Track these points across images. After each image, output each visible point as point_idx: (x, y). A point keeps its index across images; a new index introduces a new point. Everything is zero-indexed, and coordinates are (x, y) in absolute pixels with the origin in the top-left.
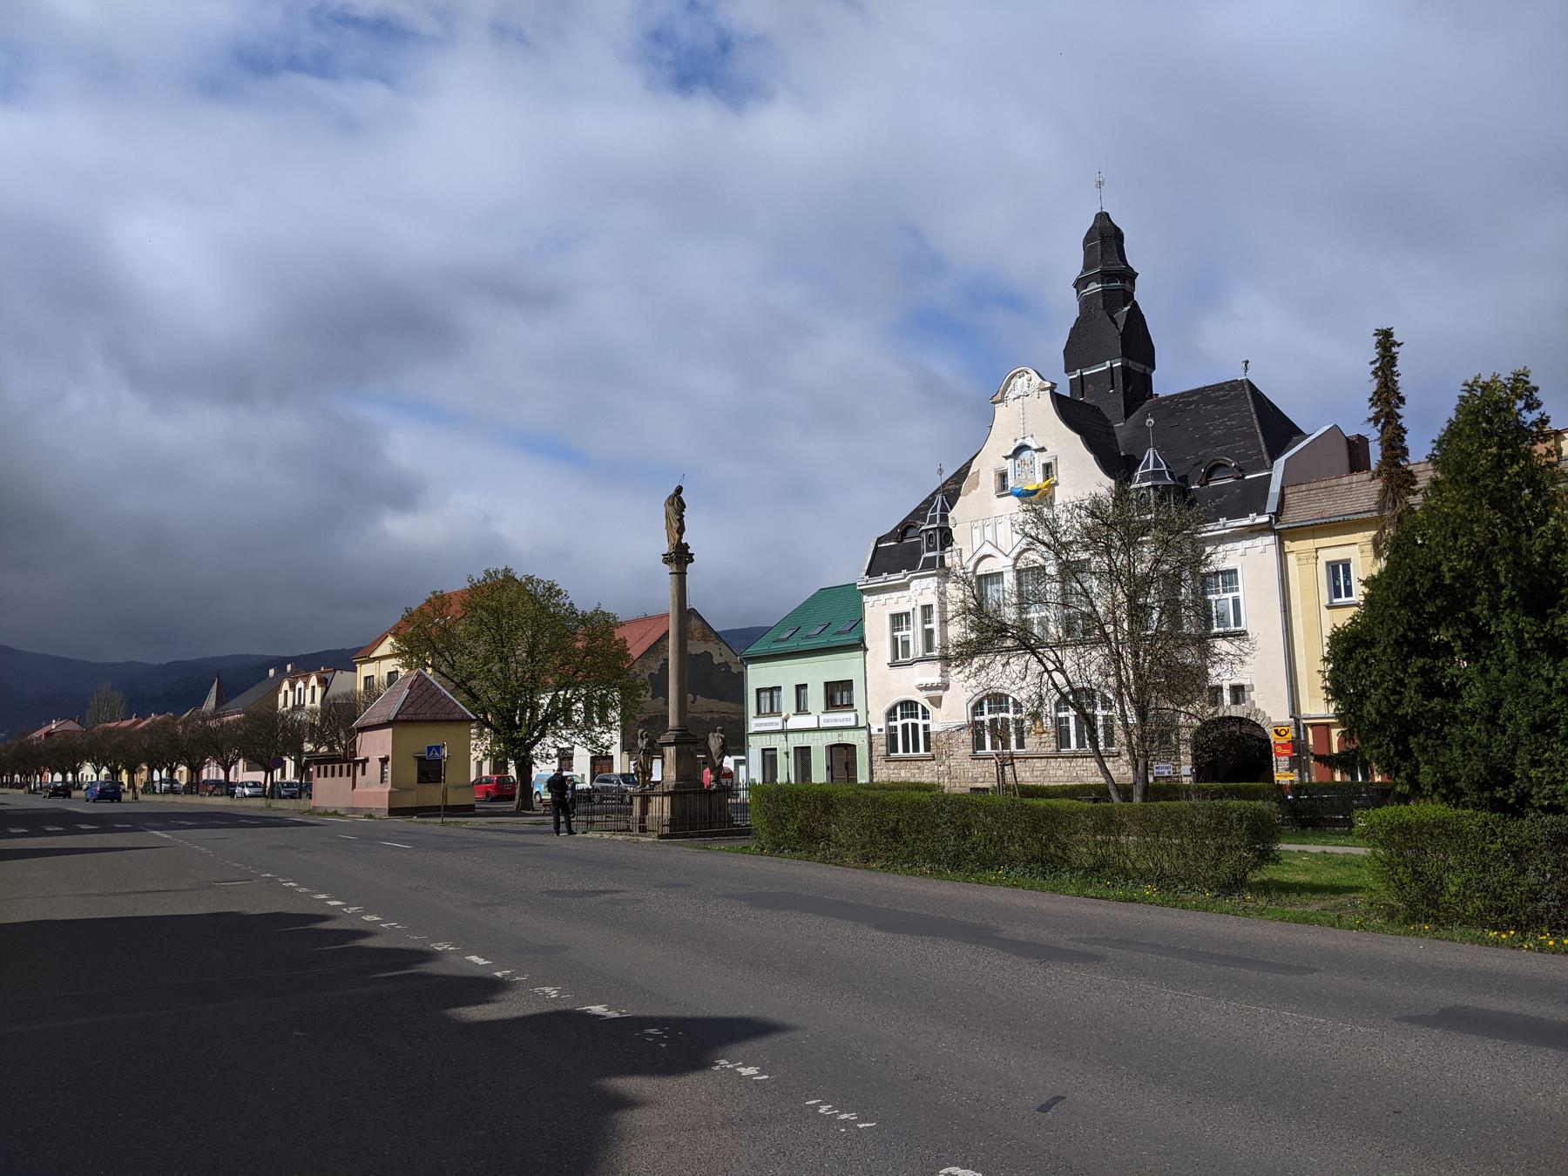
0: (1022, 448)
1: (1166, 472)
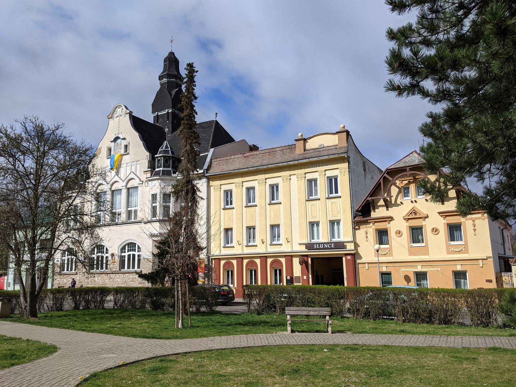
0: (117, 138)
1: (170, 151)
